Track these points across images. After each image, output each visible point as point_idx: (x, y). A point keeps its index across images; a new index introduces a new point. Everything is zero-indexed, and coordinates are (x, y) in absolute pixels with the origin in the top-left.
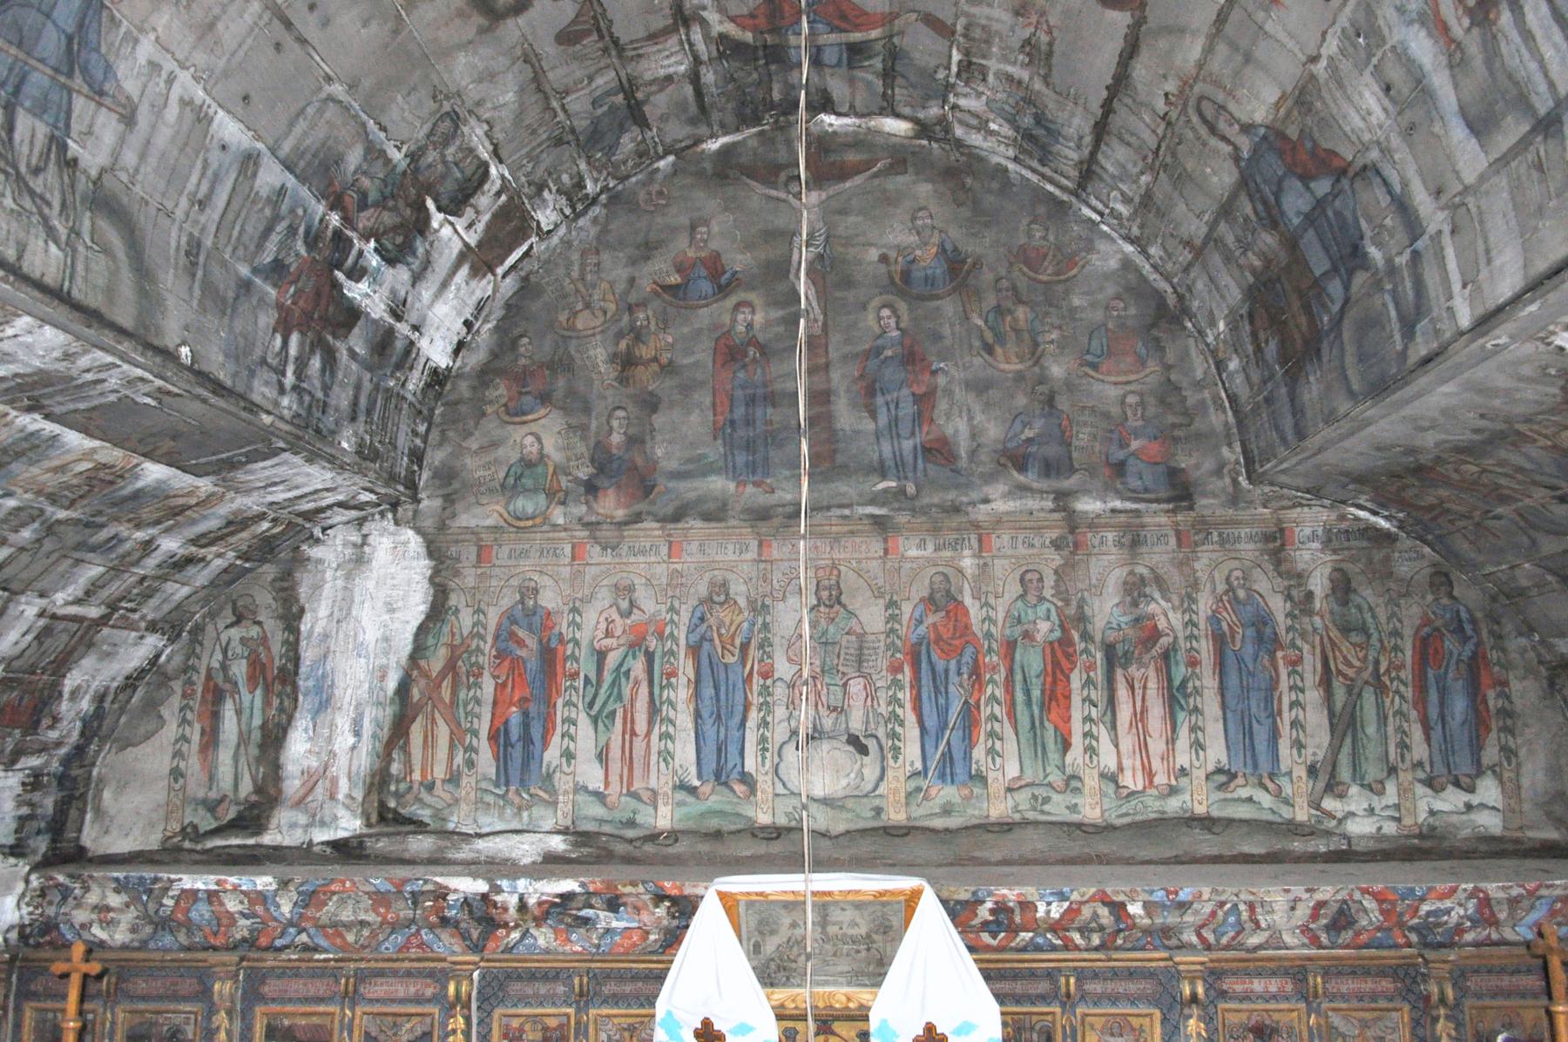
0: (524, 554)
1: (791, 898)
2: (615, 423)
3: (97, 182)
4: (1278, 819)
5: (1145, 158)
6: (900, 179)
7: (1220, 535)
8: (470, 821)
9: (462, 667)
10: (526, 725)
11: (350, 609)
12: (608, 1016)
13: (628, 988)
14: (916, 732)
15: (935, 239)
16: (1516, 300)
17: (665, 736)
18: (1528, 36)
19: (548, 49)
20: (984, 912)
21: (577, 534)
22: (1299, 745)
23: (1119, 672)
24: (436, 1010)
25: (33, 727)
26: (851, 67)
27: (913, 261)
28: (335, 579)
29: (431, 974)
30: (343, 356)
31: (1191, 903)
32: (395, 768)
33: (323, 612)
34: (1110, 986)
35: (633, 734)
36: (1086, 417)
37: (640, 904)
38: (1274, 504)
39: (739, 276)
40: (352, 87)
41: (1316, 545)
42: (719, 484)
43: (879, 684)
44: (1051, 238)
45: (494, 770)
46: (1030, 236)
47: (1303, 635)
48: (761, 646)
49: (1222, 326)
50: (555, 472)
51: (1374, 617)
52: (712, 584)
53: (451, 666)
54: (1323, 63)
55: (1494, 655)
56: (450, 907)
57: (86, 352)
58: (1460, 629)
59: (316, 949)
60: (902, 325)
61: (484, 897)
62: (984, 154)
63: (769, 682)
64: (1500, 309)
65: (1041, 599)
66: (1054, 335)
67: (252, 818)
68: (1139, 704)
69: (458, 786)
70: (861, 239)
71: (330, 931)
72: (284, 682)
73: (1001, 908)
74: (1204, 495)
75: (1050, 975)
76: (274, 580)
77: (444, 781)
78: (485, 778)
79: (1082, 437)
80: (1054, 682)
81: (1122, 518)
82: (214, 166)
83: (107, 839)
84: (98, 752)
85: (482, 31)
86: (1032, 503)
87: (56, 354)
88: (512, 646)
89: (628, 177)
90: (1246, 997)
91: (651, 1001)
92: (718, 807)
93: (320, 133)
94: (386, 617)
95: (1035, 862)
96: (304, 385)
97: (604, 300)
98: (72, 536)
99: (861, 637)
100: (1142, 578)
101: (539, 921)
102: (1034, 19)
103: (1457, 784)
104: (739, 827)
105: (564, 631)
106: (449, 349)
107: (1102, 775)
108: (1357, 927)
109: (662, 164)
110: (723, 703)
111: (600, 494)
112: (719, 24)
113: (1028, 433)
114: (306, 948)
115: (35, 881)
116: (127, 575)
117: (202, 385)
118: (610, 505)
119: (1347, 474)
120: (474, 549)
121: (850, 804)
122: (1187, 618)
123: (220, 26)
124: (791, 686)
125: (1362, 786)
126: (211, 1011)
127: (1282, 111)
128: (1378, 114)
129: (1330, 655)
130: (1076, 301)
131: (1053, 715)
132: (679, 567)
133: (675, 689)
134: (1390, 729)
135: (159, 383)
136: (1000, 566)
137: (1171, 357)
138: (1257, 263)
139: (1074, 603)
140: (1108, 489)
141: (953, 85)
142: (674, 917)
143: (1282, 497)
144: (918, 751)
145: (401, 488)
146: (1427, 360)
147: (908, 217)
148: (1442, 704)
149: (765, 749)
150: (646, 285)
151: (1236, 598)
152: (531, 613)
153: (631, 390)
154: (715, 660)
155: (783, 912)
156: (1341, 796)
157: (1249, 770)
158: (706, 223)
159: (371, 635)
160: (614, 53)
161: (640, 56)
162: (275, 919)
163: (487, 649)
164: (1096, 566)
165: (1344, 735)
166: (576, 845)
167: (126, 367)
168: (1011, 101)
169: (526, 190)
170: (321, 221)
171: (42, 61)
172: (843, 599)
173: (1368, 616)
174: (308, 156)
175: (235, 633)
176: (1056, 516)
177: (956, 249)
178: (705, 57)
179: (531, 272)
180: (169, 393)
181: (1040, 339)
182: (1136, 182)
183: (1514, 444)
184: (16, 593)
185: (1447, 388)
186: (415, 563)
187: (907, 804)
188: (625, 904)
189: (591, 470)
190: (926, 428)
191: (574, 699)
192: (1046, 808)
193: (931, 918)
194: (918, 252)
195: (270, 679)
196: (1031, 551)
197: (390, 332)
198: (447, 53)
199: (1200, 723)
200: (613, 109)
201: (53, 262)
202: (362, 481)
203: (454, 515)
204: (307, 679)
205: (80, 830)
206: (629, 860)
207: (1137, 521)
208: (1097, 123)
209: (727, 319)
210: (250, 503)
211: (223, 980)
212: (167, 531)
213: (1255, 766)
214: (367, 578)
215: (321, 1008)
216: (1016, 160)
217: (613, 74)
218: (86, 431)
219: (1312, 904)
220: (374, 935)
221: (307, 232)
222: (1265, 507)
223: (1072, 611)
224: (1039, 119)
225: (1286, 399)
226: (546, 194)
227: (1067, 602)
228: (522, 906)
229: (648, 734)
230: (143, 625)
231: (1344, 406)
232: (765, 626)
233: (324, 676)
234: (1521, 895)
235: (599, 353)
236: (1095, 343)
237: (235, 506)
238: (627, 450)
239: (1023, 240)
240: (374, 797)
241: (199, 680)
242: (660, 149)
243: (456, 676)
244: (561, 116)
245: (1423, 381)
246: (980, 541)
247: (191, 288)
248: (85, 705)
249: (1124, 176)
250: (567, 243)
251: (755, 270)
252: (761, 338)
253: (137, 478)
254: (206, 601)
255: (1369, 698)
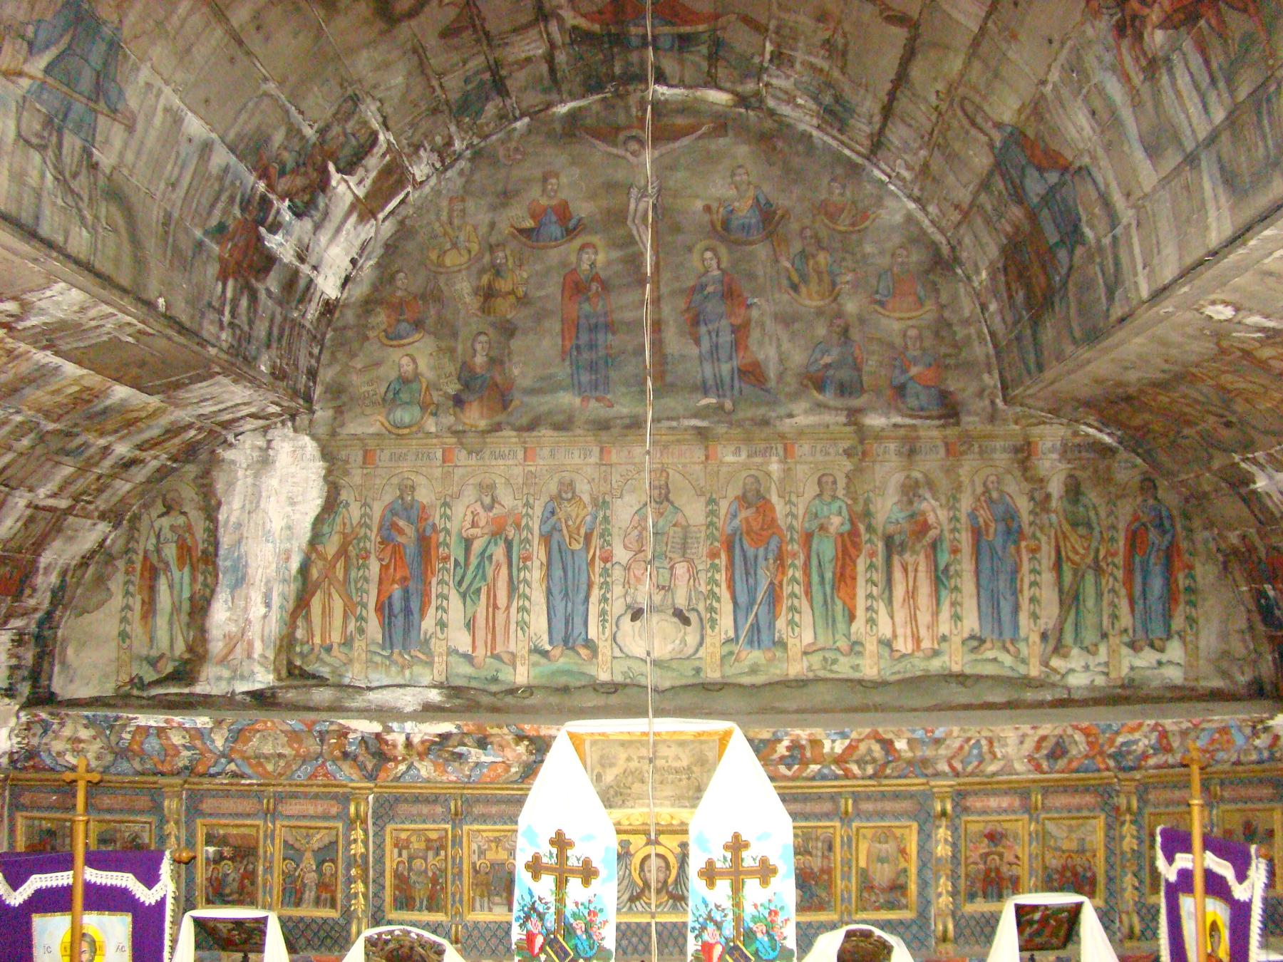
0: (401, 457)
1: (627, 737)
2: (478, 347)
3: (110, 178)
4: (1015, 675)
5: (922, 137)
6: (722, 141)
7: (980, 447)
8: (362, 676)
9: (352, 551)
10: (406, 599)
11: (258, 502)
12: (479, 831)
13: (494, 810)
14: (730, 607)
15: (751, 193)
16: (1175, 281)
17: (521, 609)
18: (1178, 94)
19: (432, 41)
20: (782, 749)
21: (447, 440)
22: (1035, 616)
23: (896, 560)
24: (340, 825)
25: (18, 596)
26: (681, 50)
27: (732, 211)
28: (246, 477)
29: (335, 797)
30: (262, 295)
31: (945, 739)
32: (300, 634)
33: (236, 504)
34: (879, 806)
35: (496, 607)
36: (875, 347)
37: (504, 743)
38: (1023, 422)
39: (585, 221)
40: (281, 84)
41: (1055, 456)
42: (567, 399)
43: (700, 567)
44: (848, 193)
45: (380, 636)
46: (831, 192)
47: (1041, 529)
48: (602, 536)
49: (984, 275)
50: (427, 388)
51: (1097, 514)
52: (561, 483)
53: (343, 552)
54: (1049, 87)
55: (1184, 545)
56: (350, 744)
57: (96, 305)
58: (1160, 525)
59: (242, 776)
60: (723, 266)
61: (378, 735)
62: (792, 122)
63: (609, 565)
64: (1165, 288)
65: (834, 498)
66: (849, 277)
67: (185, 672)
68: (911, 584)
69: (351, 647)
70: (689, 191)
71: (253, 761)
72: (206, 563)
73: (795, 746)
74: (969, 413)
75: (833, 798)
76: (196, 477)
77: (340, 645)
78: (374, 642)
79: (871, 364)
80: (843, 567)
81: (902, 432)
82: (183, 155)
83: (72, 687)
84: (61, 617)
85: (382, 33)
86: (828, 418)
87: (76, 308)
88: (394, 533)
89: (487, 136)
90: (984, 812)
91: (513, 819)
92: (567, 667)
93: (256, 121)
94: (289, 509)
95: (825, 711)
96: (236, 321)
97: (469, 241)
98: (55, 444)
99: (686, 528)
100: (917, 482)
101: (421, 756)
102: (832, 25)
103: (1152, 646)
104: (583, 683)
105: (437, 522)
106: (339, 283)
107: (880, 642)
108: (1069, 756)
109: (518, 124)
110: (570, 582)
111: (467, 406)
112: (571, 19)
113: (827, 359)
114: (235, 775)
115: (24, 717)
116: (88, 474)
117: (171, 327)
118: (475, 416)
119: (1078, 401)
120: (360, 453)
121: (674, 665)
122: (951, 514)
123: (194, 50)
124: (627, 568)
125: (1082, 648)
126: (163, 821)
127: (1023, 117)
128: (1088, 131)
129: (1062, 544)
130: (868, 248)
131: (841, 594)
132: (533, 469)
133: (530, 571)
134: (1105, 603)
135: (141, 326)
136: (801, 470)
137: (944, 298)
138: (1009, 229)
139: (861, 502)
140: (890, 407)
141: (767, 69)
142: (532, 753)
143: (1031, 416)
144: (731, 623)
145: (301, 402)
146: (1122, 320)
147: (728, 174)
148: (1145, 584)
149: (605, 621)
150: (504, 228)
151: (990, 498)
152: (408, 508)
153: (492, 318)
154: (563, 547)
155: (621, 749)
156: (1065, 656)
157: (995, 637)
158: (557, 176)
159: (277, 524)
160: (485, 43)
161: (507, 44)
162: (211, 751)
163: (373, 537)
164: (879, 471)
165: (1070, 607)
166: (449, 697)
167: (120, 315)
168: (814, 83)
169: (406, 150)
170: (252, 188)
171: (80, 93)
172: (671, 496)
173: (1092, 514)
174: (246, 140)
175: (165, 522)
176: (848, 429)
177: (768, 203)
178: (560, 43)
179: (405, 218)
180: (145, 333)
181: (838, 280)
182: (915, 154)
183: (1191, 382)
184: (13, 489)
185: (1139, 340)
186: (311, 464)
187: (722, 664)
188: (491, 743)
189: (458, 387)
190: (741, 355)
191: (446, 578)
192: (835, 667)
193: (739, 748)
194: (736, 204)
195: (195, 560)
196: (827, 458)
197: (295, 273)
198: (352, 51)
199: (959, 599)
200: (482, 84)
201: (84, 242)
202: (272, 396)
203: (342, 425)
204: (225, 560)
205: (50, 678)
206: (495, 709)
207: (914, 434)
208: (884, 108)
209: (573, 258)
210: (183, 415)
211: (171, 798)
212: (122, 438)
213: (1001, 634)
214: (272, 476)
215: (249, 822)
216: (819, 127)
217: (482, 58)
218: (80, 363)
219: (1036, 739)
220: (288, 765)
221: (241, 203)
222: (1016, 423)
223: (859, 508)
224: (838, 99)
225: (1030, 339)
226: (422, 152)
227: (855, 500)
228: (409, 744)
229: (508, 608)
230: (96, 514)
231: (1069, 349)
232: (606, 519)
233: (239, 557)
234: (1188, 729)
235: (464, 288)
236: (882, 285)
237: (172, 418)
238: (489, 370)
239: (823, 195)
240: (283, 657)
241: (138, 559)
242: (517, 113)
243: (347, 558)
244: (439, 91)
245: (1120, 335)
246: (785, 450)
247: (165, 253)
248: (54, 579)
249: (906, 148)
250: (437, 192)
251: (598, 217)
252: (602, 274)
253: (107, 397)
254: (142, 495)
255: (1090, 578)
